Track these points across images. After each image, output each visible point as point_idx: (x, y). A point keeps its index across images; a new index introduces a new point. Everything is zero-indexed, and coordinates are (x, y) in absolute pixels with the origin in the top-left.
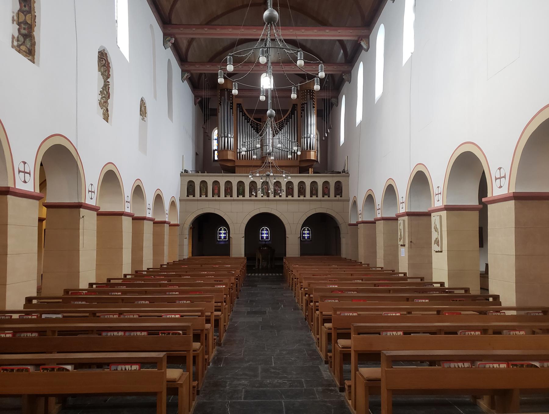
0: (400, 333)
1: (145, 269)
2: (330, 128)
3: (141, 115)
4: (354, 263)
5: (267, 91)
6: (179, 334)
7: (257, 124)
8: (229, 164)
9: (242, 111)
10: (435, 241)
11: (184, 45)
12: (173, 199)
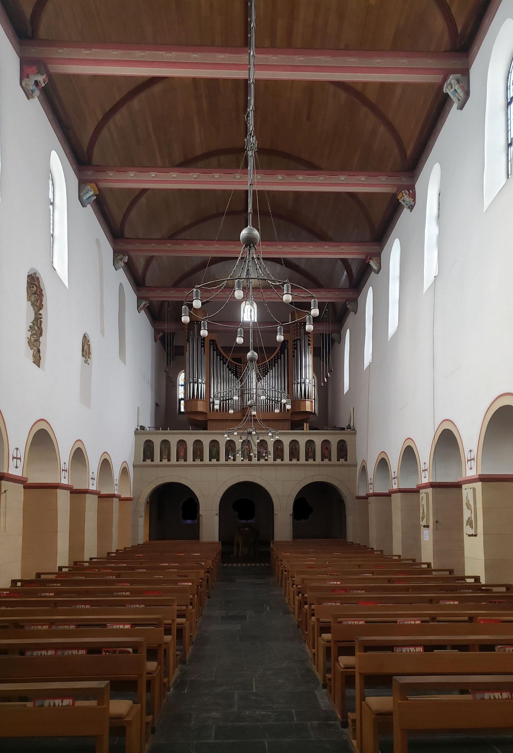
0: (420, 649)
1: (87, 559)
2: (330, 371)
3: (83, 355)
4: (363, 549)
5: (247, 324)
6: (129, 652)
7: (236, 366)
8: (199, 418)
9: (216, 349)
10: (468, 521)
11: (140, 264)
12: (125, 465)
